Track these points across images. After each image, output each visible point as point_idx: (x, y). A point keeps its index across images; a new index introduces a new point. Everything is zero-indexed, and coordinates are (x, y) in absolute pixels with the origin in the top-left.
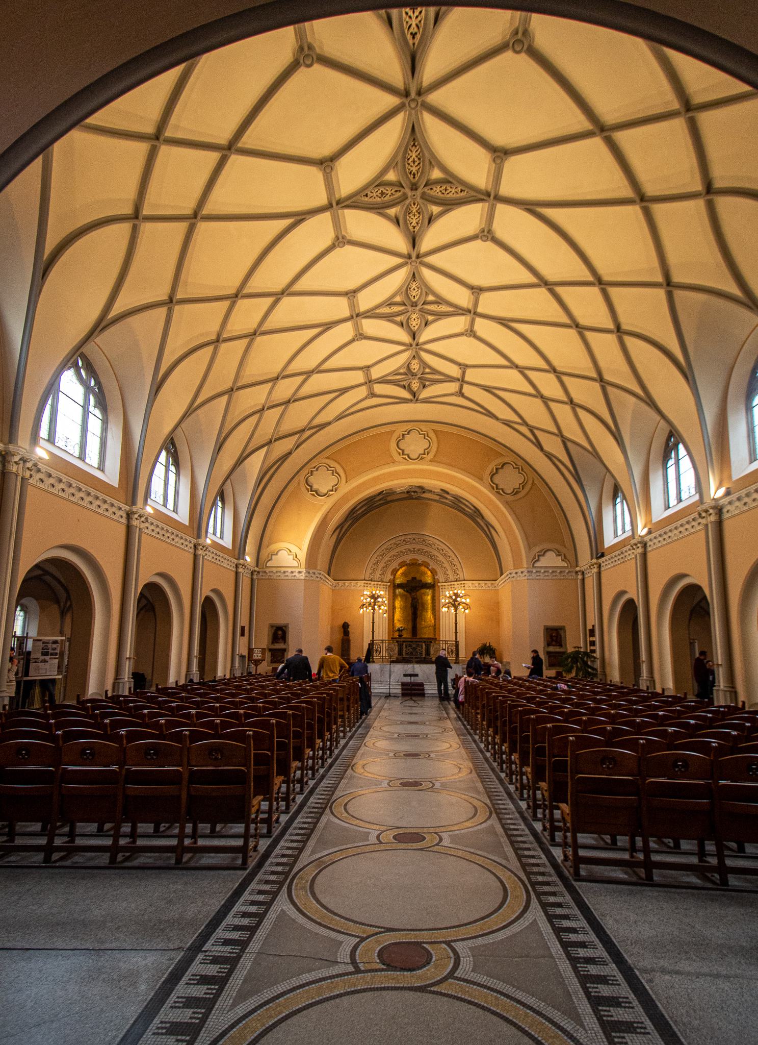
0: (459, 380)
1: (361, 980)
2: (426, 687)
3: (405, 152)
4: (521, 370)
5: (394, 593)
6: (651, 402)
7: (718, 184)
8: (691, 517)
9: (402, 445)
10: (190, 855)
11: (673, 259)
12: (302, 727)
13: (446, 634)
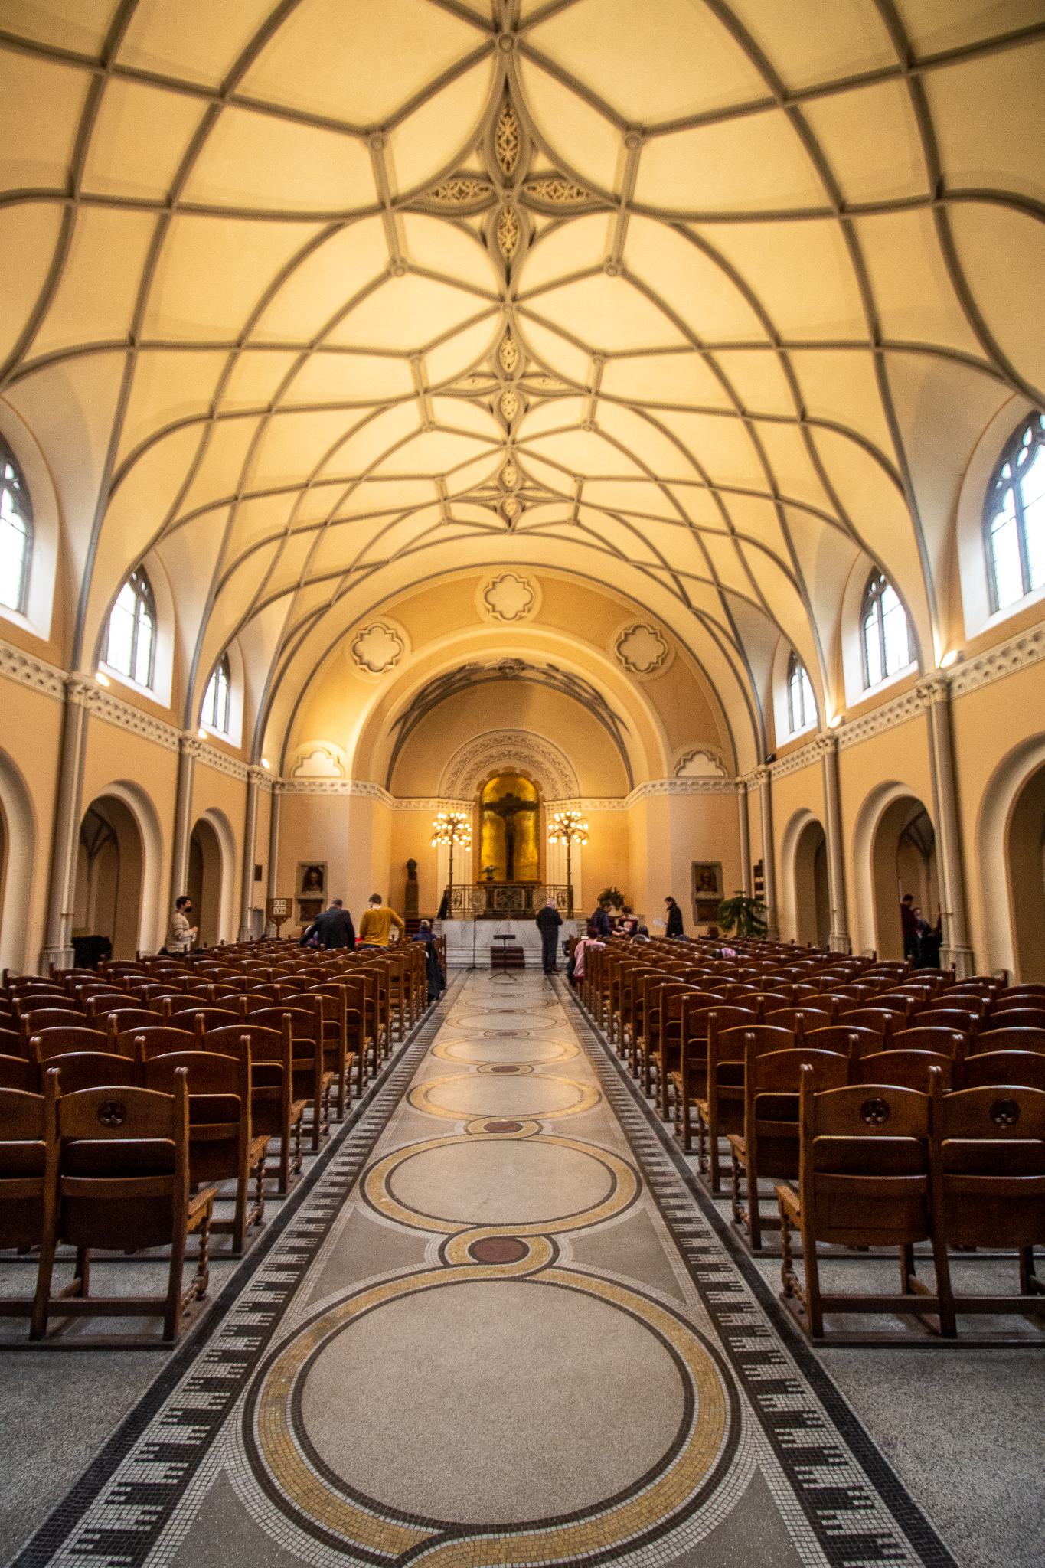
0: (572, 499)
1: (448, 1275)
2: (526, 954)
3: (495, 126)
4: (662, 483)
5: (481, 817)
6: (848, 529)
7: (953, 184)
8: (904, 698)
9: (492, 598)
10: (60, 1320)
11: (885, 304)
12: (360, 1007)
13: (555, 876)
